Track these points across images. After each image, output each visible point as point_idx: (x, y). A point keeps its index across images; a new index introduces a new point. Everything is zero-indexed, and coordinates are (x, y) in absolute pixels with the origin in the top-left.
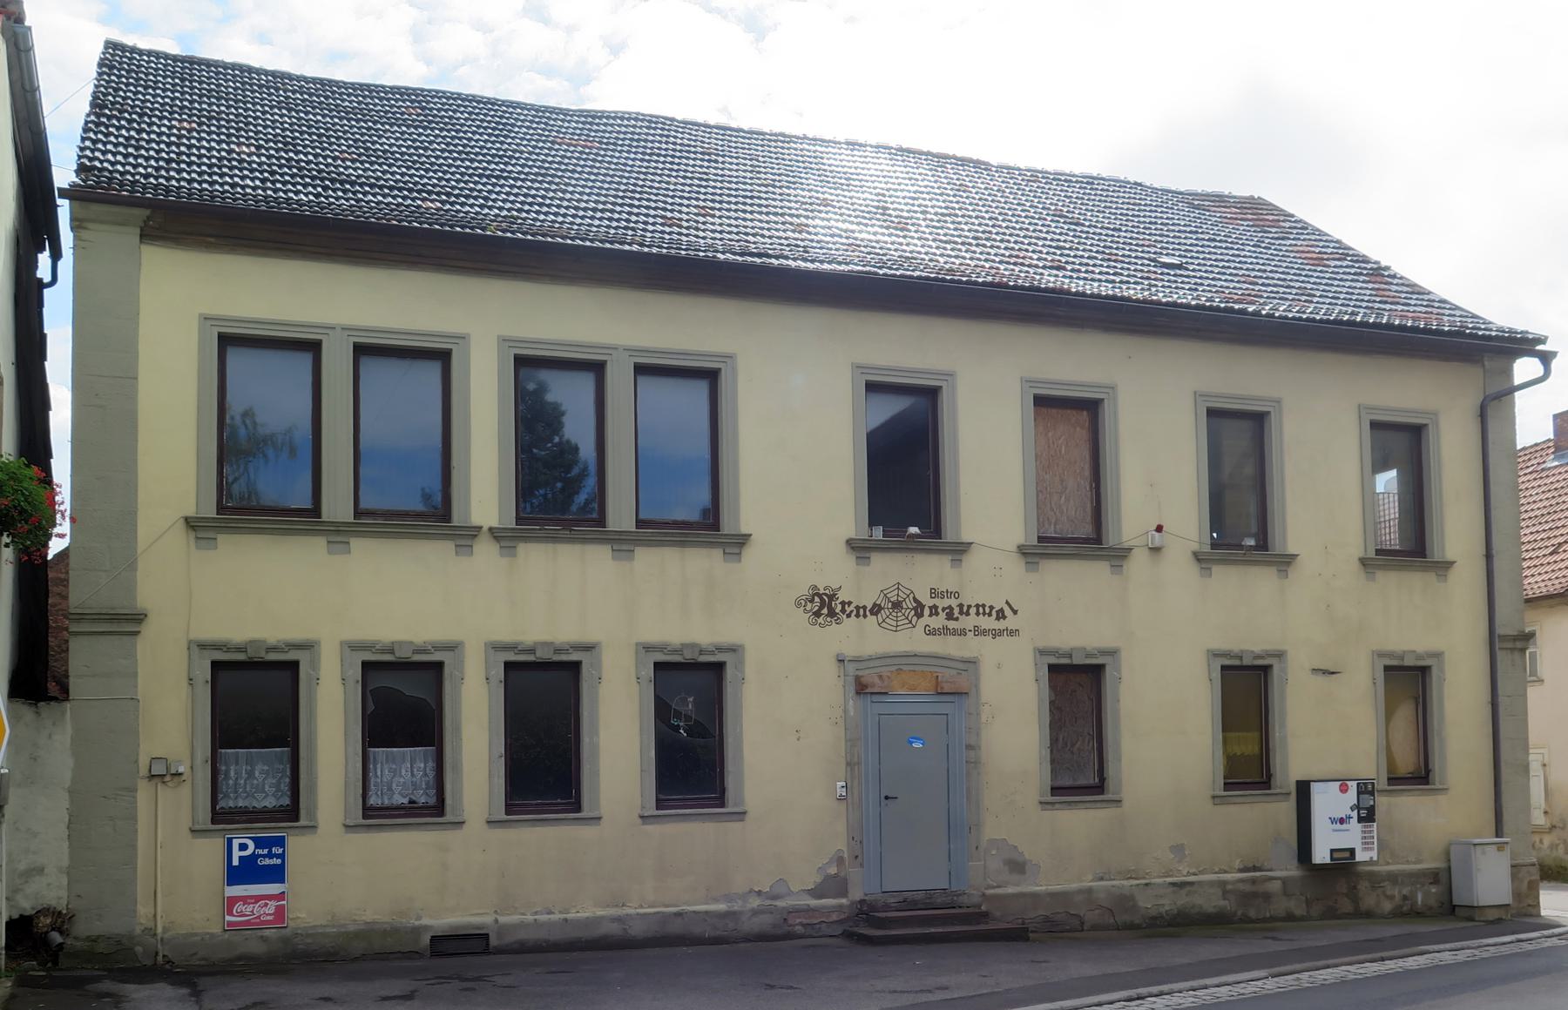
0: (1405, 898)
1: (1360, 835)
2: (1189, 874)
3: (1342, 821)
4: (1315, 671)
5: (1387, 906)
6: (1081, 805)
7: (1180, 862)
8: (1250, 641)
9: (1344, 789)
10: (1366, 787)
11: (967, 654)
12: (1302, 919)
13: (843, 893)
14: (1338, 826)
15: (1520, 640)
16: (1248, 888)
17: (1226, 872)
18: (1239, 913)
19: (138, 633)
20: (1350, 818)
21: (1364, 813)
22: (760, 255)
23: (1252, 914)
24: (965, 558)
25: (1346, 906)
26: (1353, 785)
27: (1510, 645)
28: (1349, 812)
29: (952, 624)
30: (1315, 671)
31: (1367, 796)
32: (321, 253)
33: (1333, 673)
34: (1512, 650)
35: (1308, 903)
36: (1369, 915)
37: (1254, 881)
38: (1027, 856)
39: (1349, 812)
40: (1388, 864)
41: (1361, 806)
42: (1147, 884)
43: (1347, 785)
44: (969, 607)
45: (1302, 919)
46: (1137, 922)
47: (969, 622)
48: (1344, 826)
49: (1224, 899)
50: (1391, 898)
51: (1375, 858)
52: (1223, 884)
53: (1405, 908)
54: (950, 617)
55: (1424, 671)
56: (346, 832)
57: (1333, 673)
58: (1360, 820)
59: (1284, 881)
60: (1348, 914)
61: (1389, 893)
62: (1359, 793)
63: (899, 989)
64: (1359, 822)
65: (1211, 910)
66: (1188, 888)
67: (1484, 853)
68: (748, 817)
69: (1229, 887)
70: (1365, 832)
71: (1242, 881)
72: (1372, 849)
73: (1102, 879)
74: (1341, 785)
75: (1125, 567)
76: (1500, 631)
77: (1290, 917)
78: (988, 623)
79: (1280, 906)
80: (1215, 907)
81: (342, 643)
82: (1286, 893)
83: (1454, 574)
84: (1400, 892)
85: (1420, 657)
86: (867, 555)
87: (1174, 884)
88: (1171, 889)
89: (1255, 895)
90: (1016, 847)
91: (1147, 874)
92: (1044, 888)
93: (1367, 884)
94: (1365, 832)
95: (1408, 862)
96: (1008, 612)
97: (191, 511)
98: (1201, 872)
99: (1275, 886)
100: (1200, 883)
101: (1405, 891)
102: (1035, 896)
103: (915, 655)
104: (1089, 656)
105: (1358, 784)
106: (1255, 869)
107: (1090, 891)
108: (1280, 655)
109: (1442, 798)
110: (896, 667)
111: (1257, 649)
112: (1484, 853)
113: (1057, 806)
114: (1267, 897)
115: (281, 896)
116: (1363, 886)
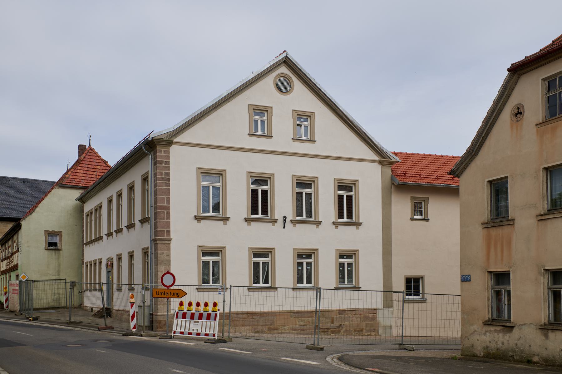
86: (274, 223)
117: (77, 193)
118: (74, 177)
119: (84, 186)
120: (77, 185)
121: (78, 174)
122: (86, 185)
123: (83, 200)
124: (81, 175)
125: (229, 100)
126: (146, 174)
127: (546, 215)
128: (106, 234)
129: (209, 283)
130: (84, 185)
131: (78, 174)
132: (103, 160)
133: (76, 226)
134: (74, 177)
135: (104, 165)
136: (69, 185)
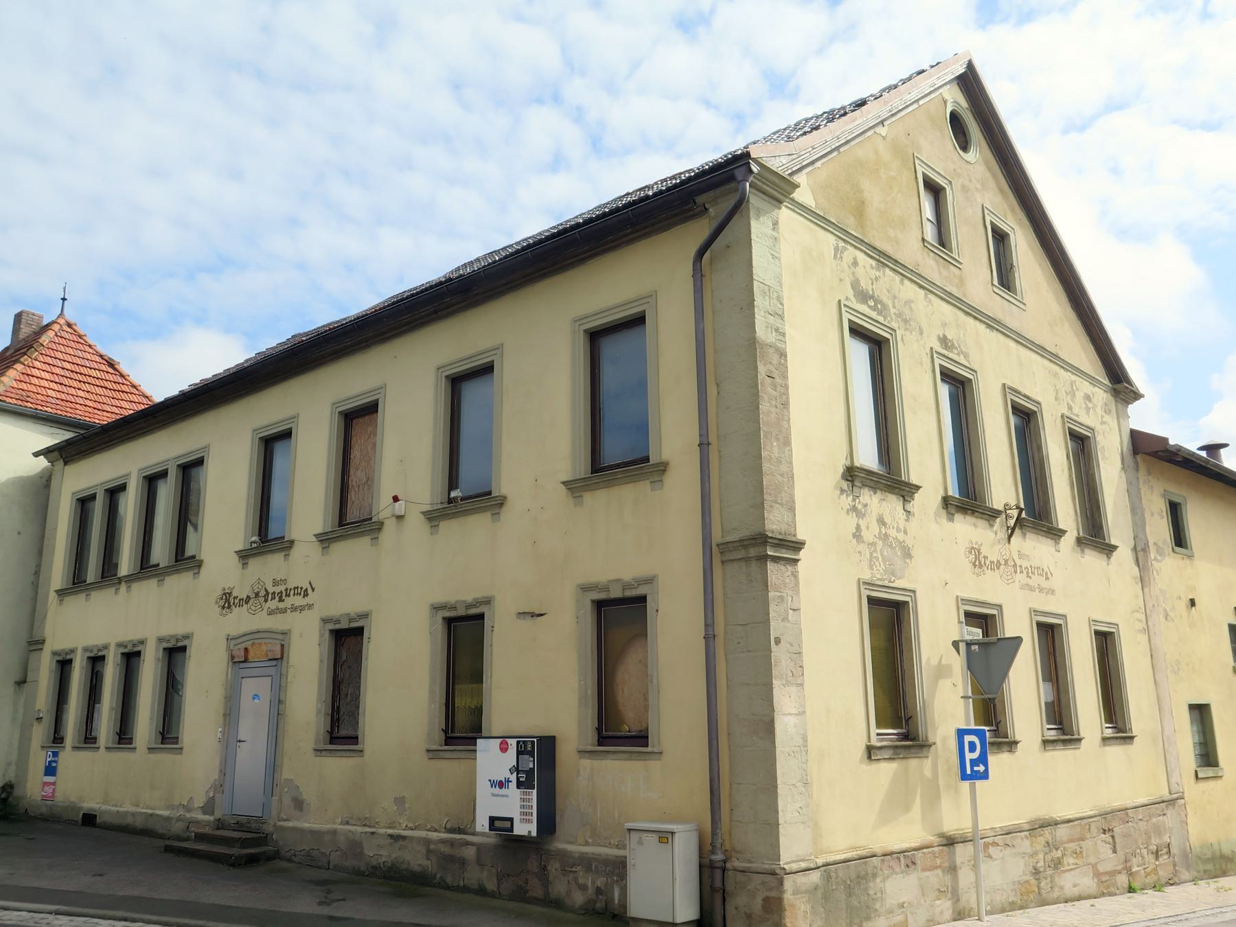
0: (599, 891)
1: (518, 803)
2: (407, 828)
3: (501, 785)
4: (522, 615)
6: (610, 756)
7: (401, 814)
8: (462, 593)
9: (504, 748)
10: (525, 746)
11: (285, 628)
12: (492, 895)
13: (212, 814)
14: (497, 790)
15: (753, 545)
16: (445, 849)
17: (436, 830)
18: (438, 876)
19: (41, 649)
20: (509, 781)
21: (523, 778)
23: (449, 880)
24: (504, 510)
25: (537, 891)
26: (513, 743)
27: (741, 554)
28: (508, 775)
29: (281, 605)
30: (522, 615)
32: (99, 450)
33: (541, 615)
34: (747, 559)
35: (500, 878)
37: (452, 843)
38: (304, 797)
39: (508, 775)
40: (587, 844)
42: (373, 833)
43: (507, 743)
44: (291, 590)
45: (492, 895)
46: (362, 868)
47: (289, 602)
48: (503, 791)
49: (428, 859)
50: (583, 888)
51: (534, 834)
52: (427, 842)
53: (598, 905)
54: (281, 600)
55: (600, 605)
56: (149, 753)
57: (541, 615)
58: (520, 785)
59: (480, 848)
60: (536, 899)
61: (581, 881)
62: (519, 753)
64: (518, 787)
65: (416, 868)
66: (401, 842)
68: (137, 750)
69: (432, 847)
71: (443, 841)
73: (347, 823)
74: (501, 743)
75: (380, 538)
77: (482, 891)
78: (298, 601)
79: (474, 876)
80: (420, 865)
81: (578, 586)
82: (479, 862)
83: (670, 479)
84: (593, 883)
85: (627, 585)
86: (376, 536)
87: (391, 836)
88: (390, 840)
89: (451, 859)
90: (298, 787)
91: (377, 823)
92: (309, 825)
93: (557, 865)
95: (610, 845)
96: (310, 591)
98: (416, 828)
99: (470, 853)
100: (412, 838)
101: (600, 882)
102: (301, 831)
103: (259, 632)
104: (351, 620)
106: (460, 831)
107: (334, 833)
108: (488, 601)
109: (653, 764)
110: (252, 642)
111: (469, 598)
112: (640, 842)
113: (324, 753)
114: (463, 862)
115: (54, 784)
116: (554, 867)
117: (48, 438)
118: (24, 386)
119: (61, 415)
120: (39, 407)
121: (35, 381)
122: (66, 412)
123: (63, 454)
124: (46, 384)
125: (192, 508)
126: (201, 451)
127: (721, 504)
128: (240, 551)
129: (986, 915)
130: (60, 412)
131: (35, 381)
132: (104, 357)
133: (19, 533)
134: (24, 386)
135: (110, 370)
136: (16, 404)
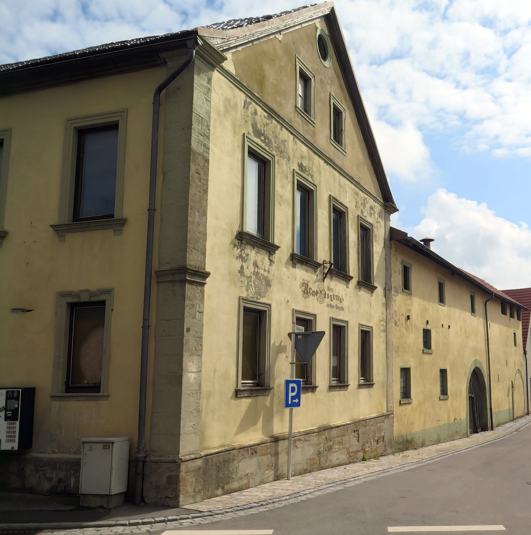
0: (60, 480)
4: (15, 310)
5: (46, 486)
10: (13, 394)
21: (10, 414)
22: (98, 226)
27: (170, 278)
30: (15, 310)
31: (13, 401)
34: (173, 282)
36: (31, 490)
40: (54, 452)
41: (8, 408)
50: (50, 479)
51: (16, 448)
53: (59, 489)
62: (7, 398)
63: (523, 426)
67: (91, 449)
70: (9, 428)
72: (13, 441)
76: (155, 266)
83: (128, 230)
94: (9, 428)
97: (290, 362)
105: (7, 392)
109: (103, 403)
112: (91, 449)
